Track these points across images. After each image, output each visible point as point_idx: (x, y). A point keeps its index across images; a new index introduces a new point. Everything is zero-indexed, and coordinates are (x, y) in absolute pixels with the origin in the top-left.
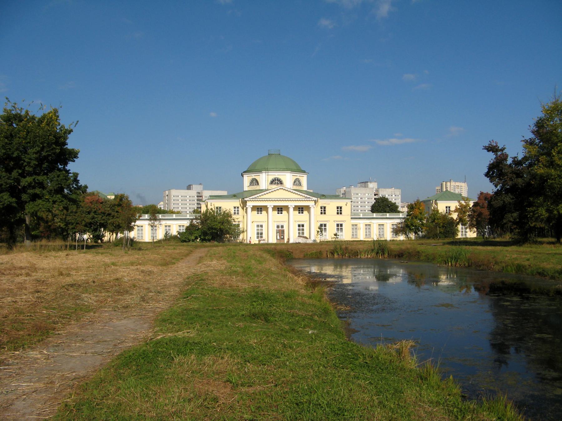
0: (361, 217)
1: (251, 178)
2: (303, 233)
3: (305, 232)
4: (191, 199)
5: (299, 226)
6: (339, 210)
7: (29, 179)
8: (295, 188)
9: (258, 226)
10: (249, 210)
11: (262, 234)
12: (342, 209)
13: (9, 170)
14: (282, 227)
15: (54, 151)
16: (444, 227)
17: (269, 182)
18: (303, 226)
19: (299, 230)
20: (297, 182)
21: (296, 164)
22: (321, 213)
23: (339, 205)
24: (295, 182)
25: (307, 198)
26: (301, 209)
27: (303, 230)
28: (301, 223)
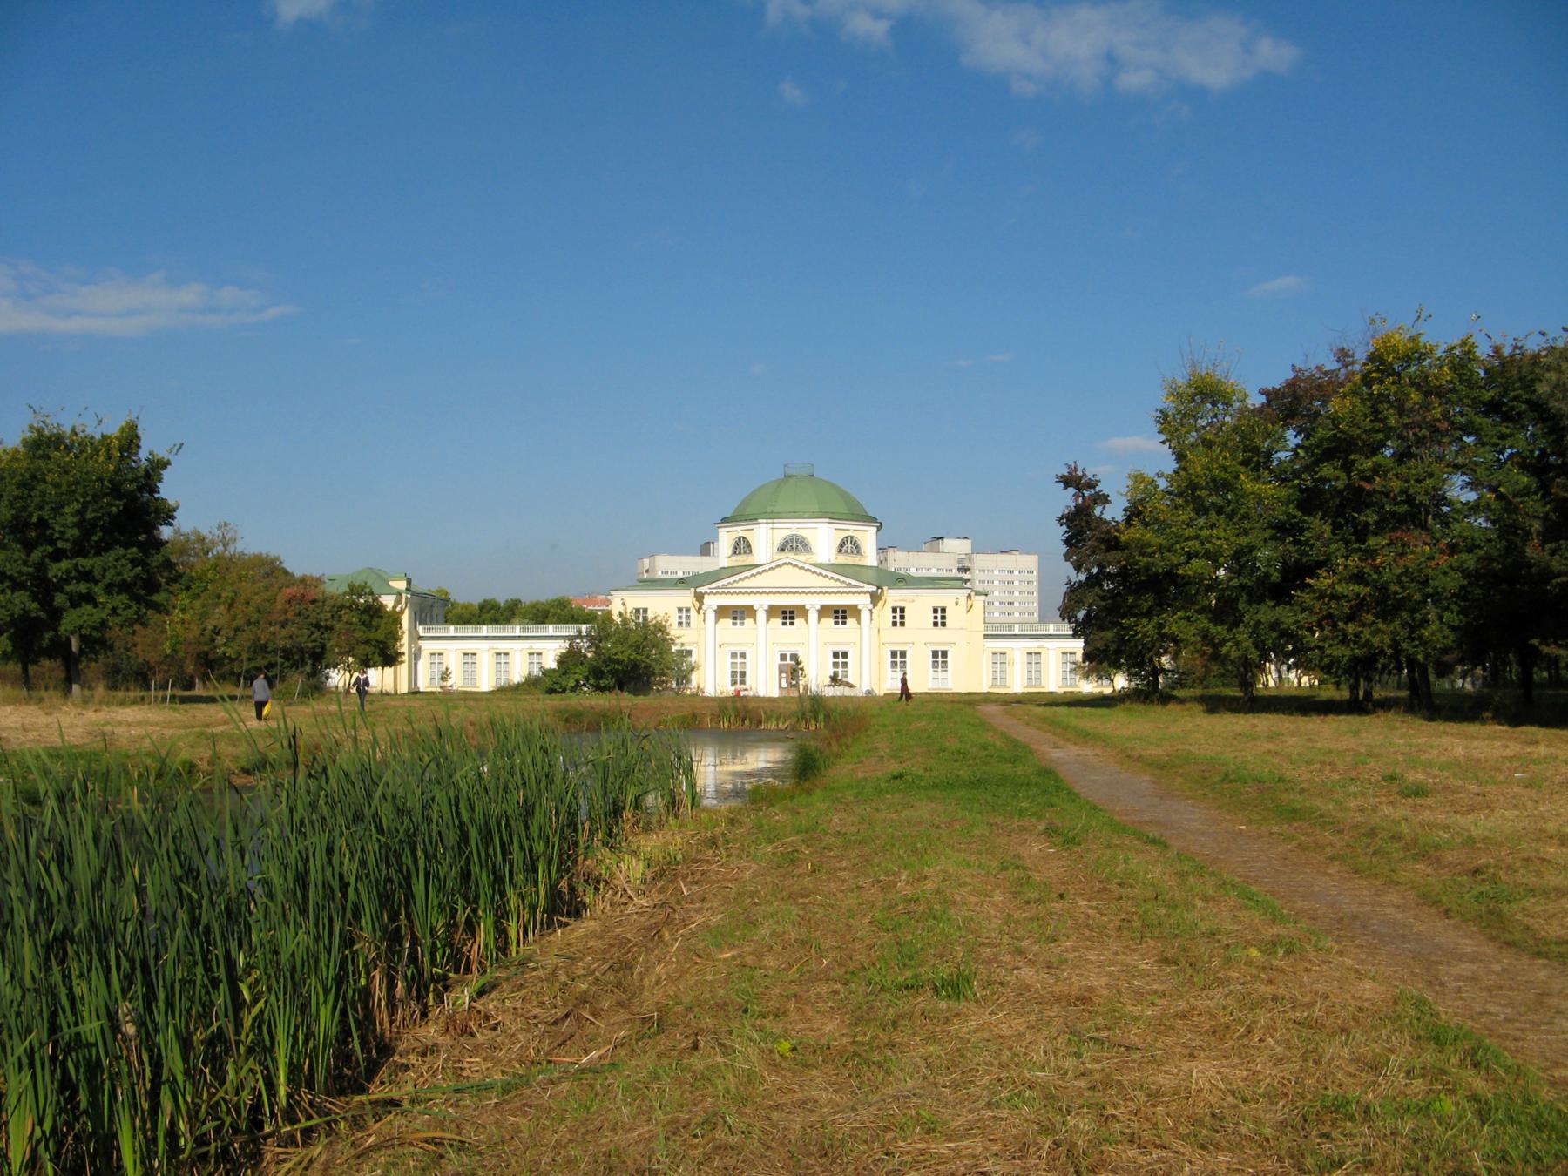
0: (1016, 632)
1: (736, 535)
3: (850, 669)
5: (836, 655)
6: (940, 617)
7: (65, 564)
8: (842, 559)
9: (734, 655)
10: (711, 616)
11: (743, 674)
13: (29, 547)
15: (122, 502)
17: (776, 545)
18: (845, 655)
19: (835, 665)
20: (848, 545)
21: (845, 497)
22: (894, 624)
24: (842, 545)
25: (849, 585)
26: (841, 614)
28: (840, 649)
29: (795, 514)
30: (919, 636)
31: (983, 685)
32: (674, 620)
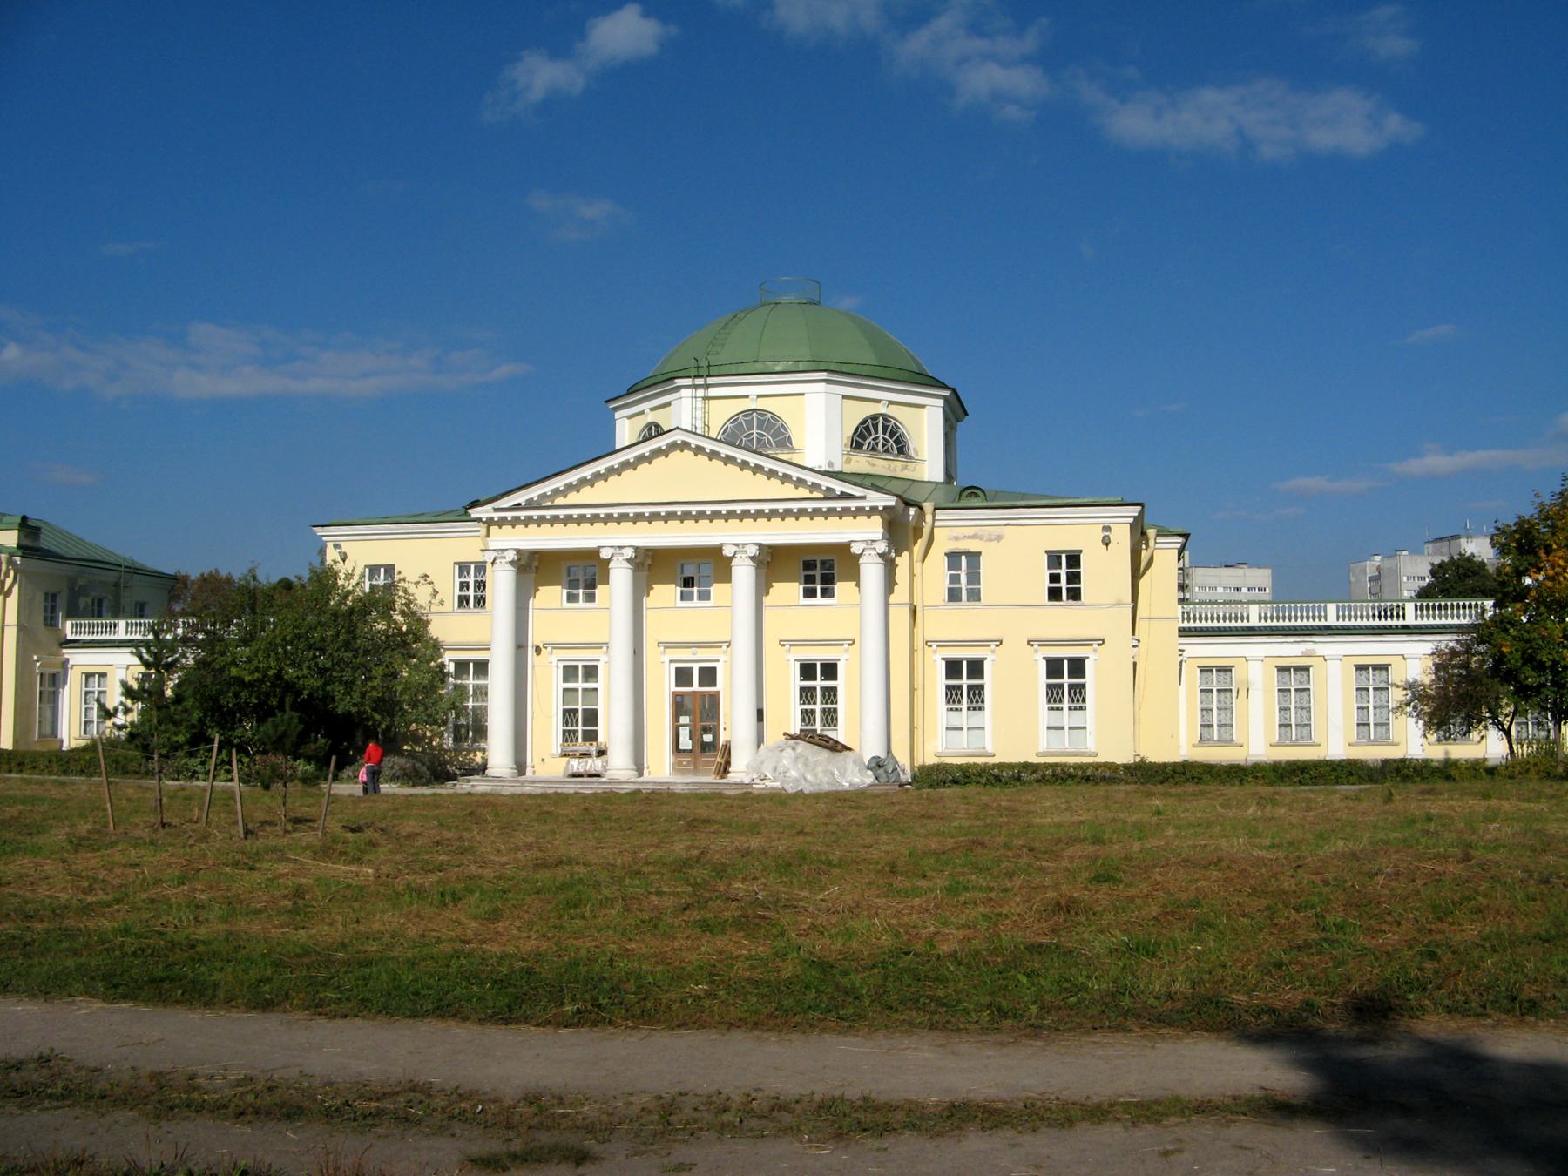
2: (831, 717)
6: (1065, 573)
8: (862, 463)
9: (570, 672)
11: (591, 717)
12: (1084, 569)
14: (709, 675)
19: (806, 694)
20: (875, 434)
23: (1064, 540)
25: (830, 495)
27: (830, 694)
29: (752, 367)
30: (1014, 622)
31: (1177, 743)
32: (449, 589)
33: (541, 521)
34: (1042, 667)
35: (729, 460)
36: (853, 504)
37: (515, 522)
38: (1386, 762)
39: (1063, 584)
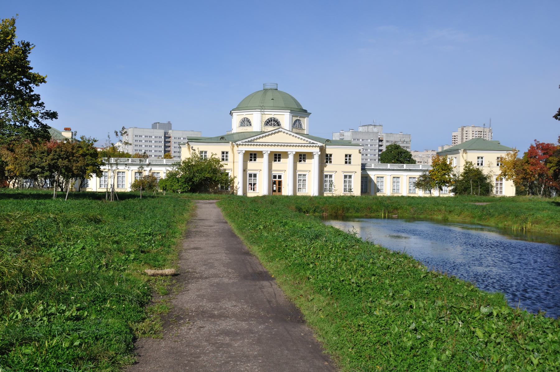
4: (158, 139)
6: (348, 159)
16: (475, 183)
19: (345, 182)
27: (350, 182)
33: (251, 145)
34: (343, 177)
35: (296, 137)
36: (315, 145)
37: (245, 145)
38: (413, 197)
39: (348, 160)
